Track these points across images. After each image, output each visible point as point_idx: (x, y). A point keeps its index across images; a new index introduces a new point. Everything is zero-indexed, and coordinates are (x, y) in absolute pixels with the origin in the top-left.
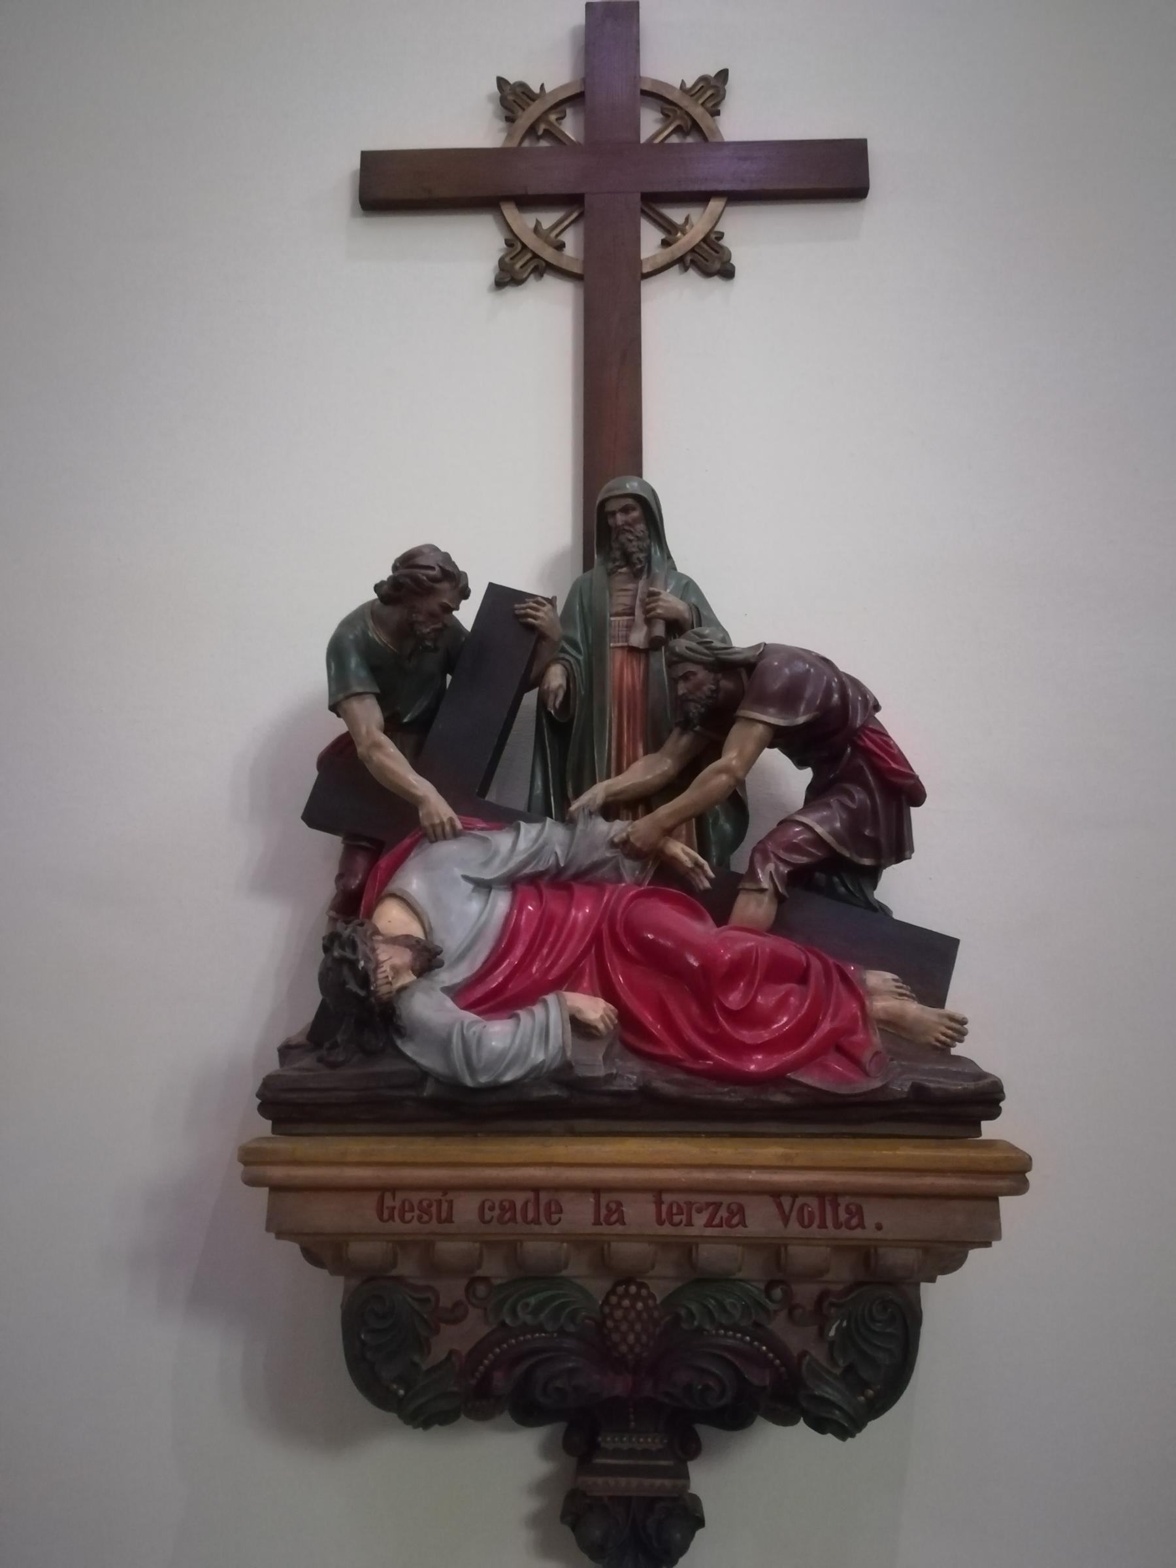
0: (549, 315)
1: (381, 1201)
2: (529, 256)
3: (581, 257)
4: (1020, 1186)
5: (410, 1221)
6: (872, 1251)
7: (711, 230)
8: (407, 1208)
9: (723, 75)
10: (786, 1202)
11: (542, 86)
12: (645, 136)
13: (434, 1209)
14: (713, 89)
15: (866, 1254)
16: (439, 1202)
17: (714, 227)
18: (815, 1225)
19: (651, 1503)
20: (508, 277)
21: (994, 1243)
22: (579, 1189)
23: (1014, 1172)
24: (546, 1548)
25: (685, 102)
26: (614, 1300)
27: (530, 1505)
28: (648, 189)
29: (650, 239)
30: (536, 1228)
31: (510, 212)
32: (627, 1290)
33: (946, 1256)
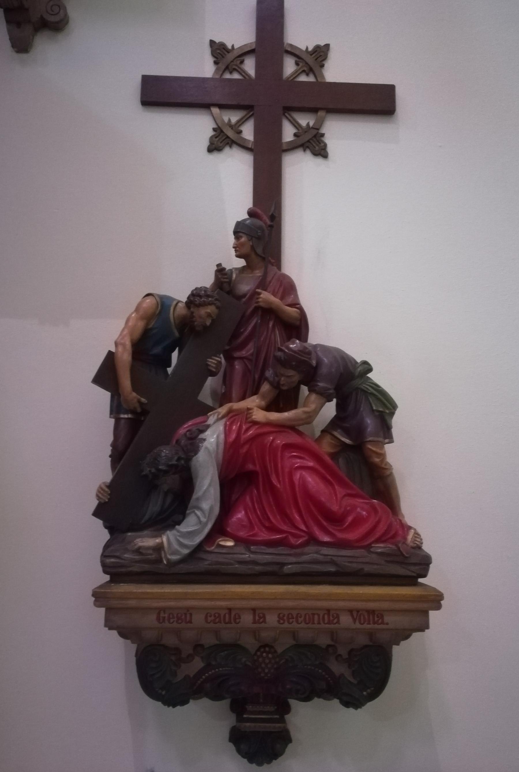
1: (159, 613)
4: (438, 607)
5: (173, 623)
8: (237, 617)
9: (327, 46)
10: (355, 614)
11: (233, 46)
13: (183, 617)
14: (321, 53)
16: (186, 614)
23: (435, 600)
26: (259, 653)
29: (288, 133)
30: (229, 626)
31: (215, 110)
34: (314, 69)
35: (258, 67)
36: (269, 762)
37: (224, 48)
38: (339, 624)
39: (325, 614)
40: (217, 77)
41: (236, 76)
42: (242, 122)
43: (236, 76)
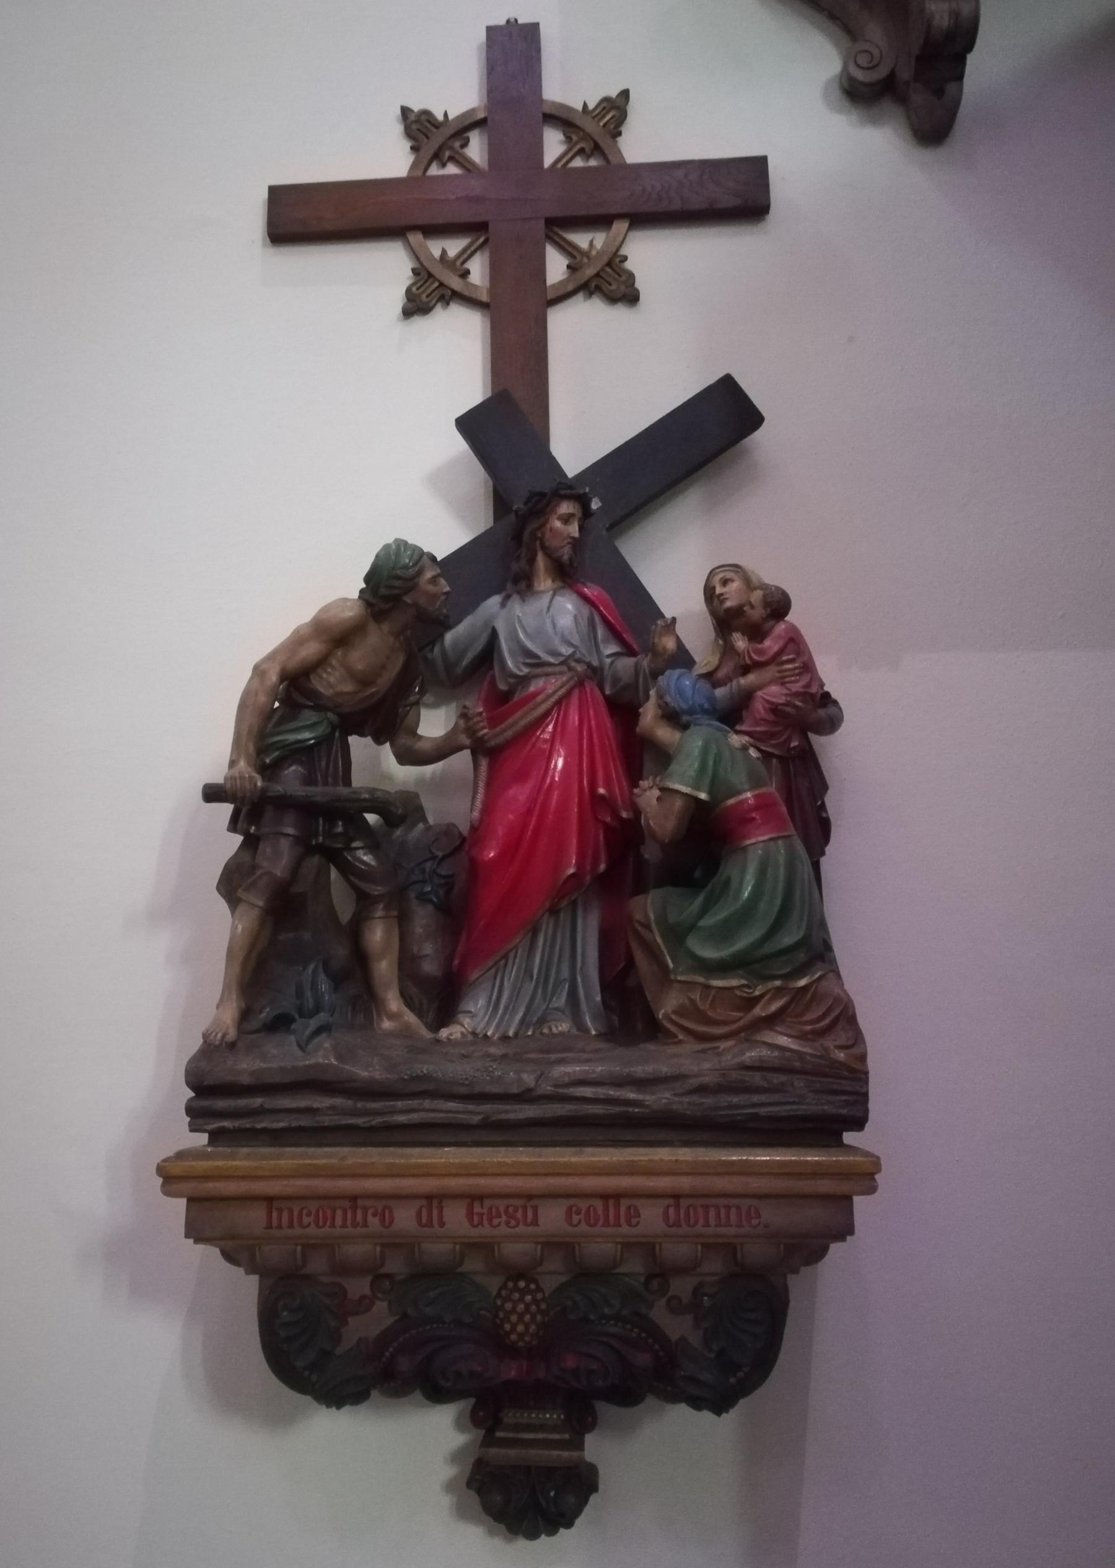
2: (436, 284)
3: (487, 284)
4: (872, 1190)
5: (498, 1225)
6: (739, 1247)
7: (616, 254)
8: (753, 1214)
9: (625, 94)
11: (446, 115)
12: (548, 161)
13: (519, 1214)
14: (615, 110)
16: (525, 1208)
17: (618, 250)
18: (601, 1222)
19: (549, 1472)
20: (416, 306)
21: (848, 1238)
25: (589, 126)
28: (556, 212)
29: (556, 267)
31: (415, 238)
32: (516, 1285)
34: (601, 144)
36: (552, 1531)
37: (429, 121)
38: (537, 1225)
39: (668, 1207)
40: (419, 173)
42: (467, 255)
43: (452, 169)
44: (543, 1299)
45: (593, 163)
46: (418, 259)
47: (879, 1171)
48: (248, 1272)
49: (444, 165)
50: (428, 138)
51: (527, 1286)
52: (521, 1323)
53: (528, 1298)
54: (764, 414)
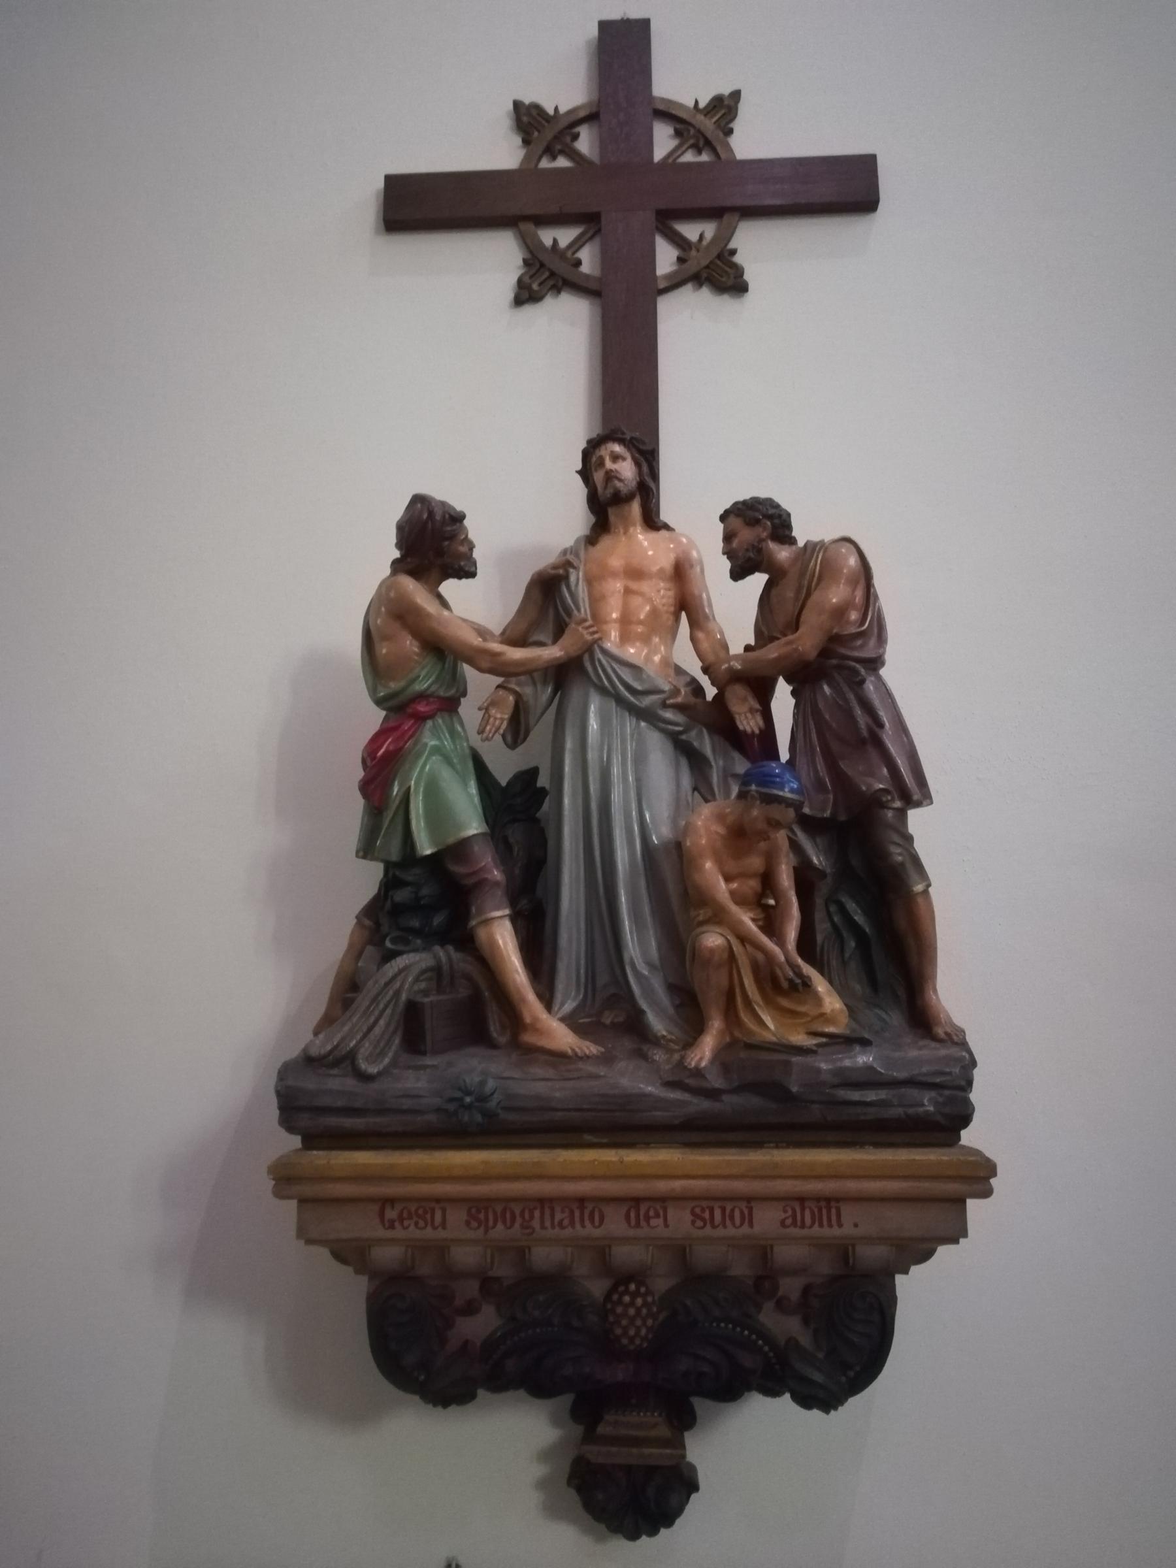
0: (567, 324)
2: (547, 274)
4: (987, 1193)
9: (736, 95)
11: (556, 109)
12: (659, 154)
14: (725, 108)
15: (844, 1252)
16: (433, 1211)
19: (651, 1470)
20: (525, 295)
21: (961, 1240)
22: (680, 1199)
23: (979, 1176)
24: (553, 1510)
25: (699, 120)
27: (539, 1470)
28: (662, 205)
29: (666, 258)
31: (528, 227)
33: (919, 1251)
35: (603, 144)
36: (653, 1532)
41: (562, 162)
43: (562, 162)
44: (654, 1302)
45: (705, 157)
46: (531, 252)
47: (994, 1174)
48: (358, 1272)
49: (554, 158)
50: (539, 131)
51: (638, 1289)
52: (636, 1325)
53: (639, 1301)
54: (740, 582)
